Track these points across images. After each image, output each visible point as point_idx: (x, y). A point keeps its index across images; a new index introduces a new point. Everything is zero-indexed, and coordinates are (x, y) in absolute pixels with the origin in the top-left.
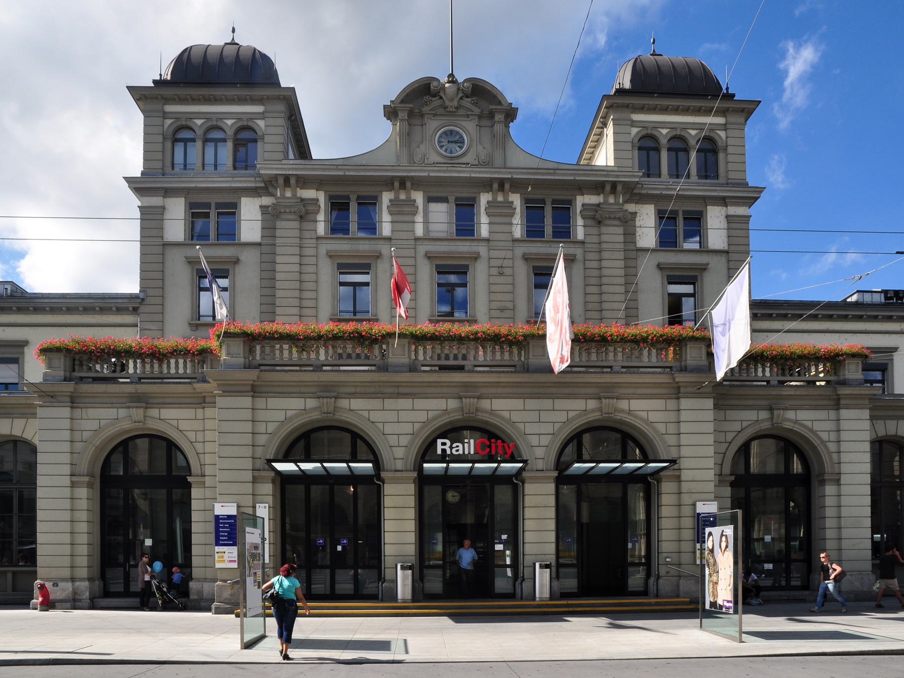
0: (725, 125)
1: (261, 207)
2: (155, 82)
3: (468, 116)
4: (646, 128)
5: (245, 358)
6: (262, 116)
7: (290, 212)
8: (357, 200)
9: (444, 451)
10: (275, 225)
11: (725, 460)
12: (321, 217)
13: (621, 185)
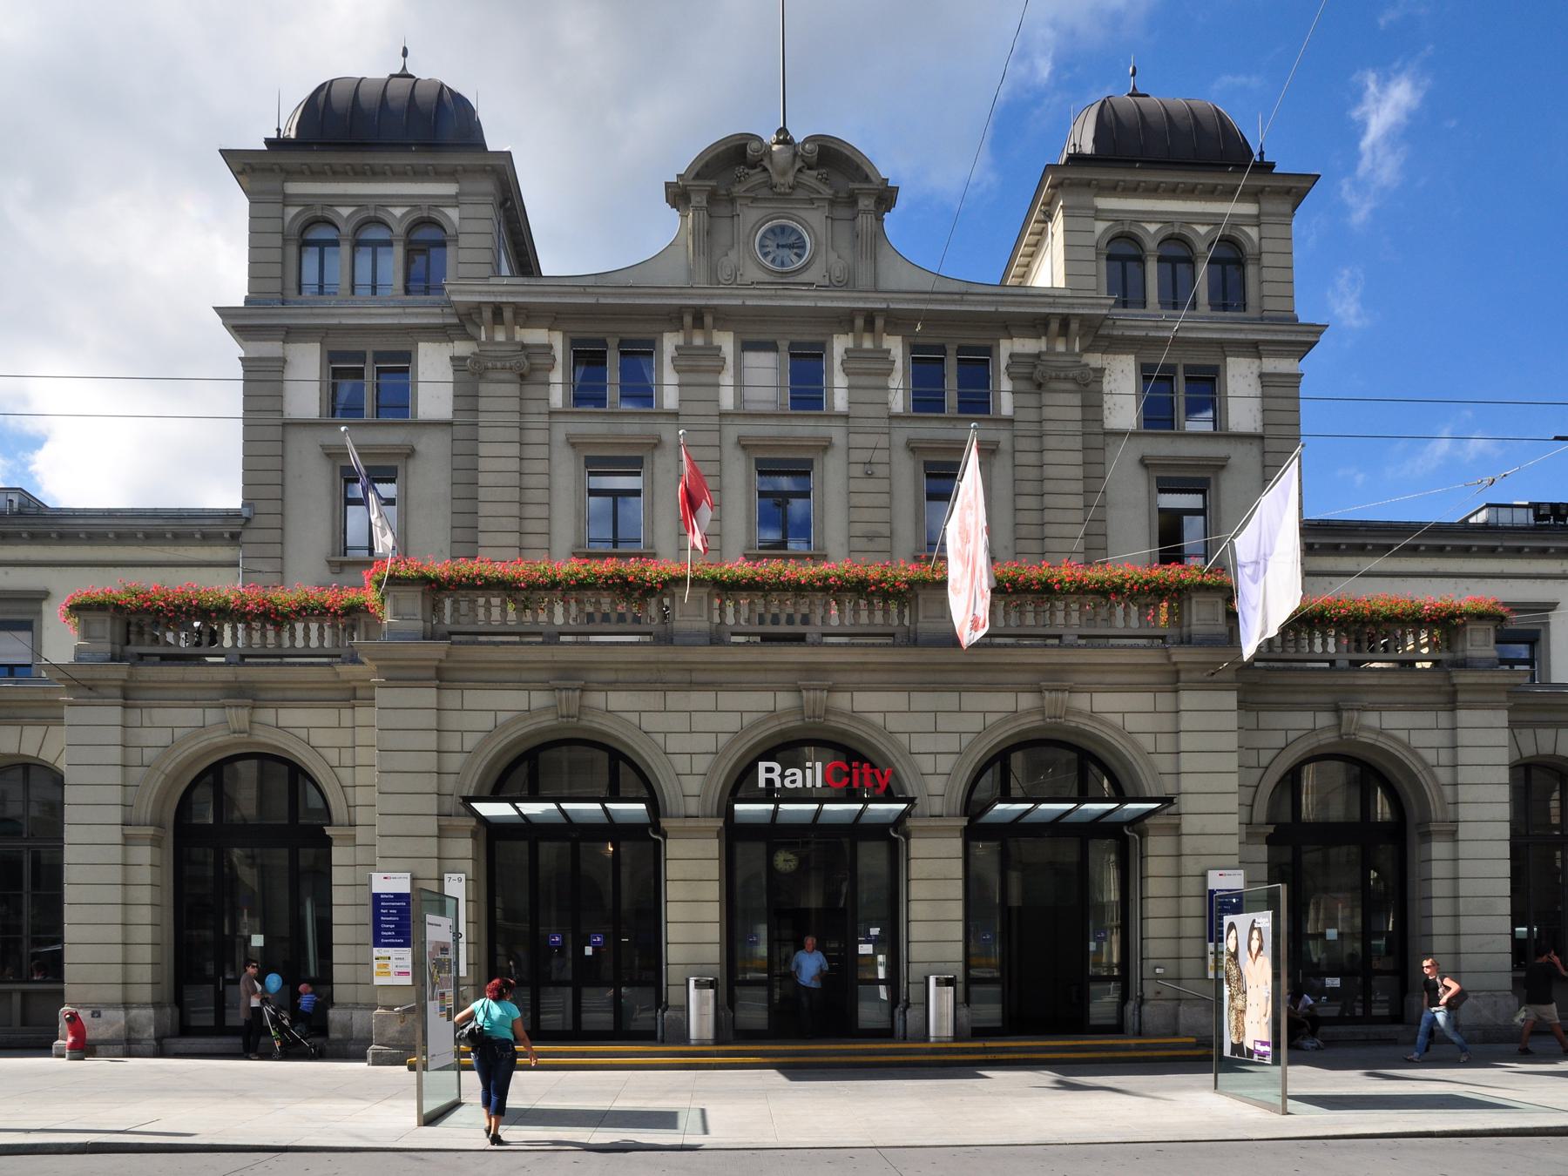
0: (1258, 216)
1: (453, 359)
2: (268, 142)
3: (811, 201)
4: (1121, 222)
5: (424, 621)
6: (455, 201)
7: (503, 368)
8: (619, 346)
9: (770, 782)
10: (477, 391)
11: (1258, 798)
12: (557, 376)
13: (1077, 321)
